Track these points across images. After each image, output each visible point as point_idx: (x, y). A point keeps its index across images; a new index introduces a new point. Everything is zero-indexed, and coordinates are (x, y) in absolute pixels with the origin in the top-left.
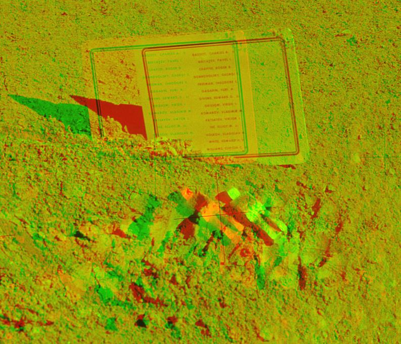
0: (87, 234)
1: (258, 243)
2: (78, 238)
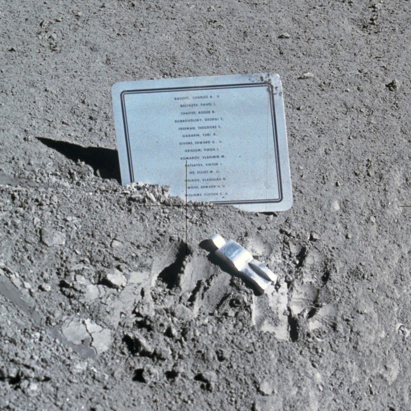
0: (73, 284)
1: (247, 293)
2: (64, 289)
